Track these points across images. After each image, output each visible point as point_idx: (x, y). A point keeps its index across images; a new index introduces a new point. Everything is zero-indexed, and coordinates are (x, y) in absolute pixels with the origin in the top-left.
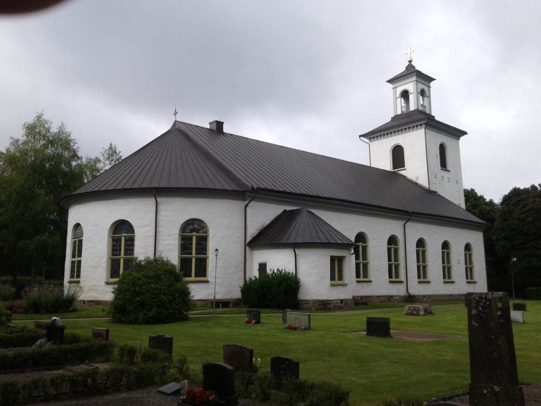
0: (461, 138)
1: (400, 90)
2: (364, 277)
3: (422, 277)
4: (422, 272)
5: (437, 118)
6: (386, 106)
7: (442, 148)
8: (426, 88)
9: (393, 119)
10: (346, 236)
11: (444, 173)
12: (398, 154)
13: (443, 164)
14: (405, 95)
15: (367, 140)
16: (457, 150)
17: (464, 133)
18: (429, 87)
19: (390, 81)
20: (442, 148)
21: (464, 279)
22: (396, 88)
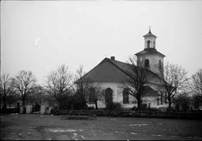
1: (147, 40)
5: (157, 50)
6: (141, 47)
9: (145, 49)
12: (147, 62)
18: (155, 40)
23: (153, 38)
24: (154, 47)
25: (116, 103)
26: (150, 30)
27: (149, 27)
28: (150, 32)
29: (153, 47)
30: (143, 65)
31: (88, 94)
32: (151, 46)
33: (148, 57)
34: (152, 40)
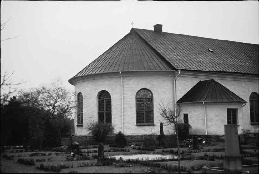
3: (255, 121)
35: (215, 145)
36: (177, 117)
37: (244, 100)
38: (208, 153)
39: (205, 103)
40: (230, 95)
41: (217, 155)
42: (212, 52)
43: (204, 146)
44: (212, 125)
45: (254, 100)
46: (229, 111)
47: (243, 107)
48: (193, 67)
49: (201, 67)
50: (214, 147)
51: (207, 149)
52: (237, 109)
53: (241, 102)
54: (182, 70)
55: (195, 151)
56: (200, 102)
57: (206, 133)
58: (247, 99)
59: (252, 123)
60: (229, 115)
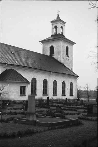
0: (74, 45)
1: (54, 25)
2: (55, 94)
3: (45, 93)
4: (55, 93)
5: (66, 37)
6: (48, 33)
7: (67, 48)
8: (63, 26)
9: (52, 36)
10: (97, 16)
11: (67, 58)
12: (52, 49)
13: (67, 54)
14: (56, 27)
15: (42, 43)
16: (72, 50)
17: (75, 43)
18: (64, 25)
19: (51, 22)
20: (67, 48)
21: (69, 95)
22: (53, 25)
23: (60, 23)
24: (62, 33)
25: (54, 99)
26: (58, 15)
27: (57, 11)
28: (58, 17)
29: (61, 33)
30: (48, 54)
31: (75, 101)
32: (59, 32)
33: (54, 45)
34: (59, 25)
35: (14, 106)
36: (2, 90)
37: (29, 82)
38: (12, 111)
39: (9, 82)
40: (23, 79)
41: (17, 112)
42: (13, 54)
43: (7, 107)
44: (12, 95)
45: (33, 82)
46: (21, 87)
47: (29, 86)
48: (42, 69)
49: (7, 62)
50: (13, 107)
51: (10, 108)
52: (25, 87)
53: (28, 82)
54: (53, 72)
55: (4, 109)
56: (6, 81)
57: (8, 99)
58: (31, 82)
59: (44, 94)
60: (21, 89)
